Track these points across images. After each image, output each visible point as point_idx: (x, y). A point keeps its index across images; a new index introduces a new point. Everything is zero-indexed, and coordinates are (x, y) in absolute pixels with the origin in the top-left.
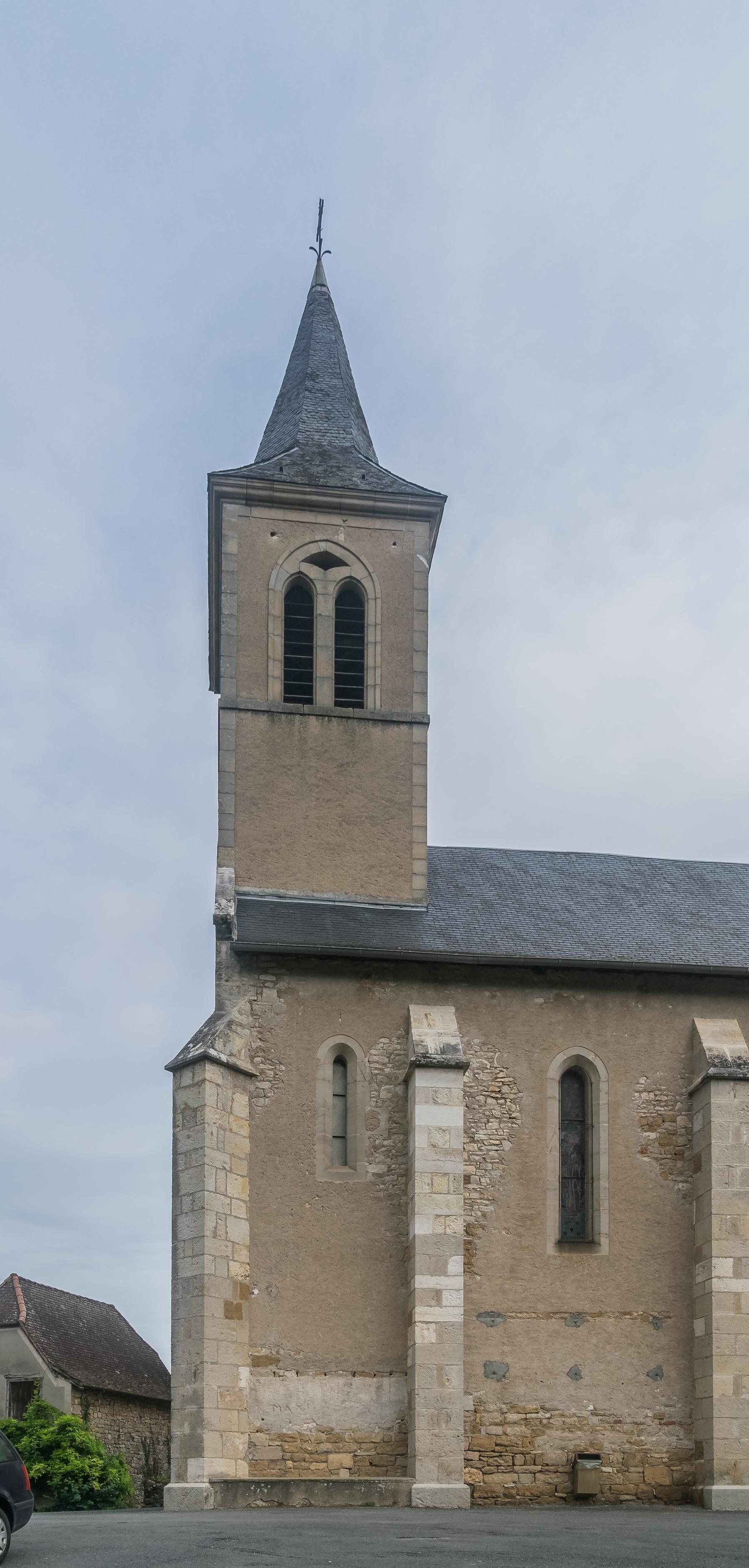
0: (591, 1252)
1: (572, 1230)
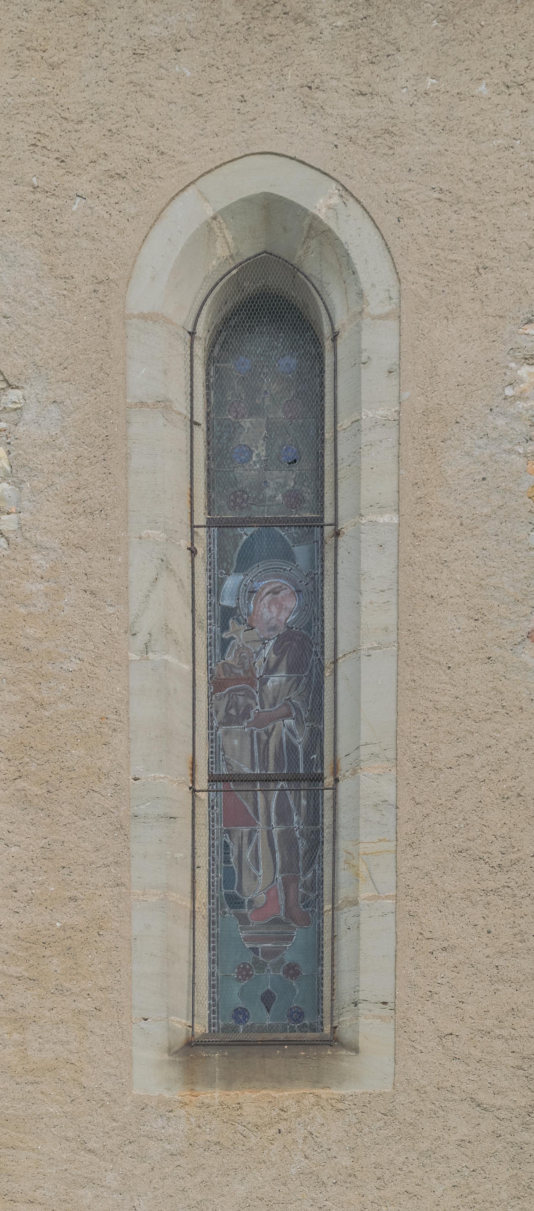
0: (317, 1081)
1: (268, 999)
